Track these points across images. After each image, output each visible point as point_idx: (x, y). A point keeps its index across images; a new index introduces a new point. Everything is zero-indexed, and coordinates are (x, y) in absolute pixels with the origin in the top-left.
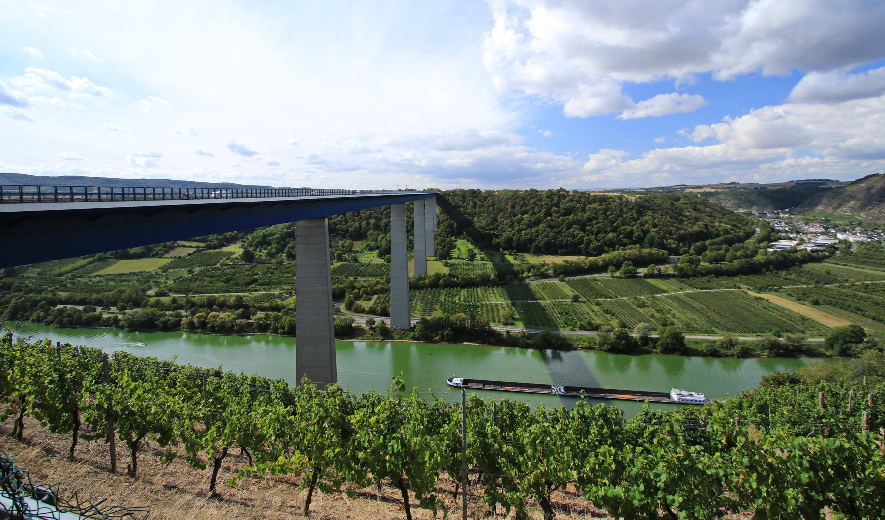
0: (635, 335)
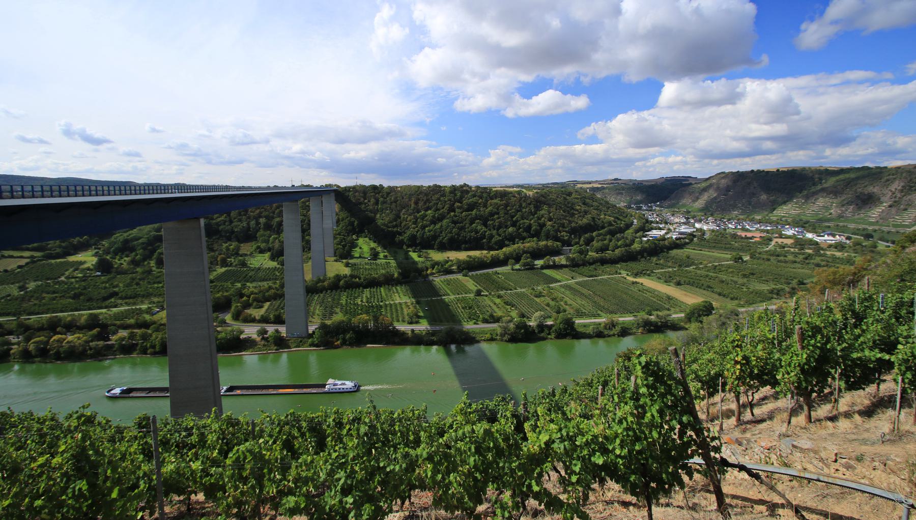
0: (532, 323)
